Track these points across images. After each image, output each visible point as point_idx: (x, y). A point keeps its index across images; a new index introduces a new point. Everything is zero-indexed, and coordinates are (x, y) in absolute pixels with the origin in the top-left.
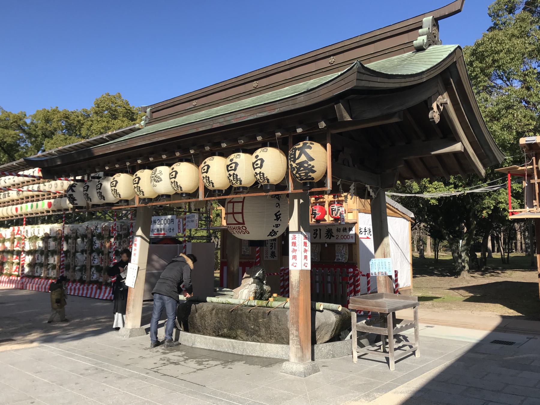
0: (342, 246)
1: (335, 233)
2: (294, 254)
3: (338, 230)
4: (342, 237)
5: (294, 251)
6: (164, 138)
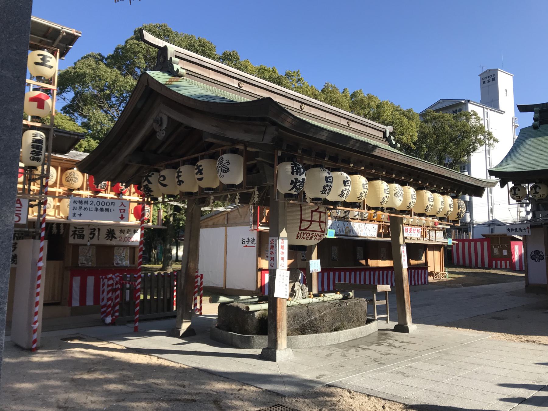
0: (122, 248)
1: (117, 234)
2: (272, 256)
3: (122, 231)
4: (126, 239)
5: (283, 253)
6: (433, 171)
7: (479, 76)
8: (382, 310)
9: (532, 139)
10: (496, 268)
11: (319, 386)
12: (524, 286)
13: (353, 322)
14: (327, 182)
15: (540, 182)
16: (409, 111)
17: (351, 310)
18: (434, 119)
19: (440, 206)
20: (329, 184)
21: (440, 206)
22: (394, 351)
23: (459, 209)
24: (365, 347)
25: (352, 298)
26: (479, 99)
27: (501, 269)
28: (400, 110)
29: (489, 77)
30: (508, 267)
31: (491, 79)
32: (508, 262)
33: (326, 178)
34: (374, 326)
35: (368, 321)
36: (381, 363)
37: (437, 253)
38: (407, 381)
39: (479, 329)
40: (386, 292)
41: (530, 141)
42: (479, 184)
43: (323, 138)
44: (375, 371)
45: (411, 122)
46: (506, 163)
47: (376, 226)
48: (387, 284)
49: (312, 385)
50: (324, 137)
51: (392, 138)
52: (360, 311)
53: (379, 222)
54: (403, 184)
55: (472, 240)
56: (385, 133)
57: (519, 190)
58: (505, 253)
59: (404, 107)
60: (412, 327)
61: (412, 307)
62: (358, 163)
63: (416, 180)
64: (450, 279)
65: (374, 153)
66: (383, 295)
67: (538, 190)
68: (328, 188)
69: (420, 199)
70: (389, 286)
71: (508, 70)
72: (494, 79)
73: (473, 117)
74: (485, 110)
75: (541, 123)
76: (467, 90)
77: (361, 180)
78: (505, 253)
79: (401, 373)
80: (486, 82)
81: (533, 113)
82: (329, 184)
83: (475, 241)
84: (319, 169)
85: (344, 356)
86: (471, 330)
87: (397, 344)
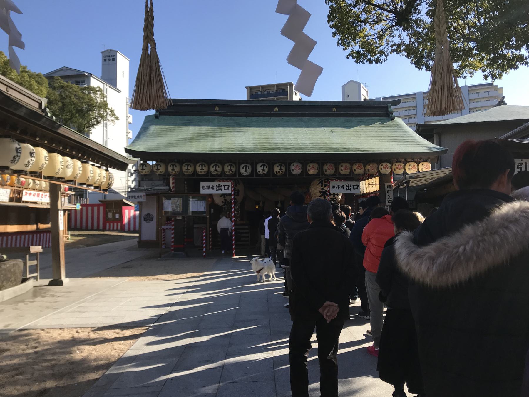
6: (97, 149)
7: (102, 53)
8: (33, 269)
9: (155, 126)
10: (109, 230)
11: (12, 332)
12: (136, 243)
13: (11, 281)
14: (17, 152)
15: (161, 162)
17: (10, 271)
18: (62, 87)
19: (97, 177)
20: (19, 154)
21: (97, 177)
22: (59, 299)
24: (32, 300)
25: (6, 260)
26: (100, 74)
27: (113, 230)
29: (109, 56)
30: (119, 228)
31: (111, 58)
32: (119, 224)
33: (17, 149)
34: (30, 284)
35: (24, 280)
36: (55, 309)
38: (84, 315)
39: (117, 276)
40: (37, 253)
41: (153, 128)
42: (126, 161)
43: (22, 114)
44: (54, 314)
46: (137, 144)
47: (9, 191)
48: (39, 245)
49: (7, 332)
50: (22, 113)
51: (48, 110)
52: (17, 271)
53: (12, 186)
54: (73, 157)
55: (90, 205)
56: (40, 104)
57: (146, 166)
58: (117, 216)
60: (65, 280)
61: (66, 263)
62: (43, 137)
63: (83, 155)
64: (72, 241)
65: (59, 131)
66: (34, 256)
67: (159, 168)
68: (17, 158)
69: (84, 170)
70: (40, 247)
71: (126, 54)
72: (114, 59)
73: (99, 93)
74: (105, 86)
75: (160, 114)
76: (89, 63)
77: (43, 152)
78: (117, 216)
79: (76, 312)
80: (107, 60)
82: (19, 154)
83: (92, 206)
84: (8, 140)
85: (16, 309)
86: (111, 278)
87: (58, 294)
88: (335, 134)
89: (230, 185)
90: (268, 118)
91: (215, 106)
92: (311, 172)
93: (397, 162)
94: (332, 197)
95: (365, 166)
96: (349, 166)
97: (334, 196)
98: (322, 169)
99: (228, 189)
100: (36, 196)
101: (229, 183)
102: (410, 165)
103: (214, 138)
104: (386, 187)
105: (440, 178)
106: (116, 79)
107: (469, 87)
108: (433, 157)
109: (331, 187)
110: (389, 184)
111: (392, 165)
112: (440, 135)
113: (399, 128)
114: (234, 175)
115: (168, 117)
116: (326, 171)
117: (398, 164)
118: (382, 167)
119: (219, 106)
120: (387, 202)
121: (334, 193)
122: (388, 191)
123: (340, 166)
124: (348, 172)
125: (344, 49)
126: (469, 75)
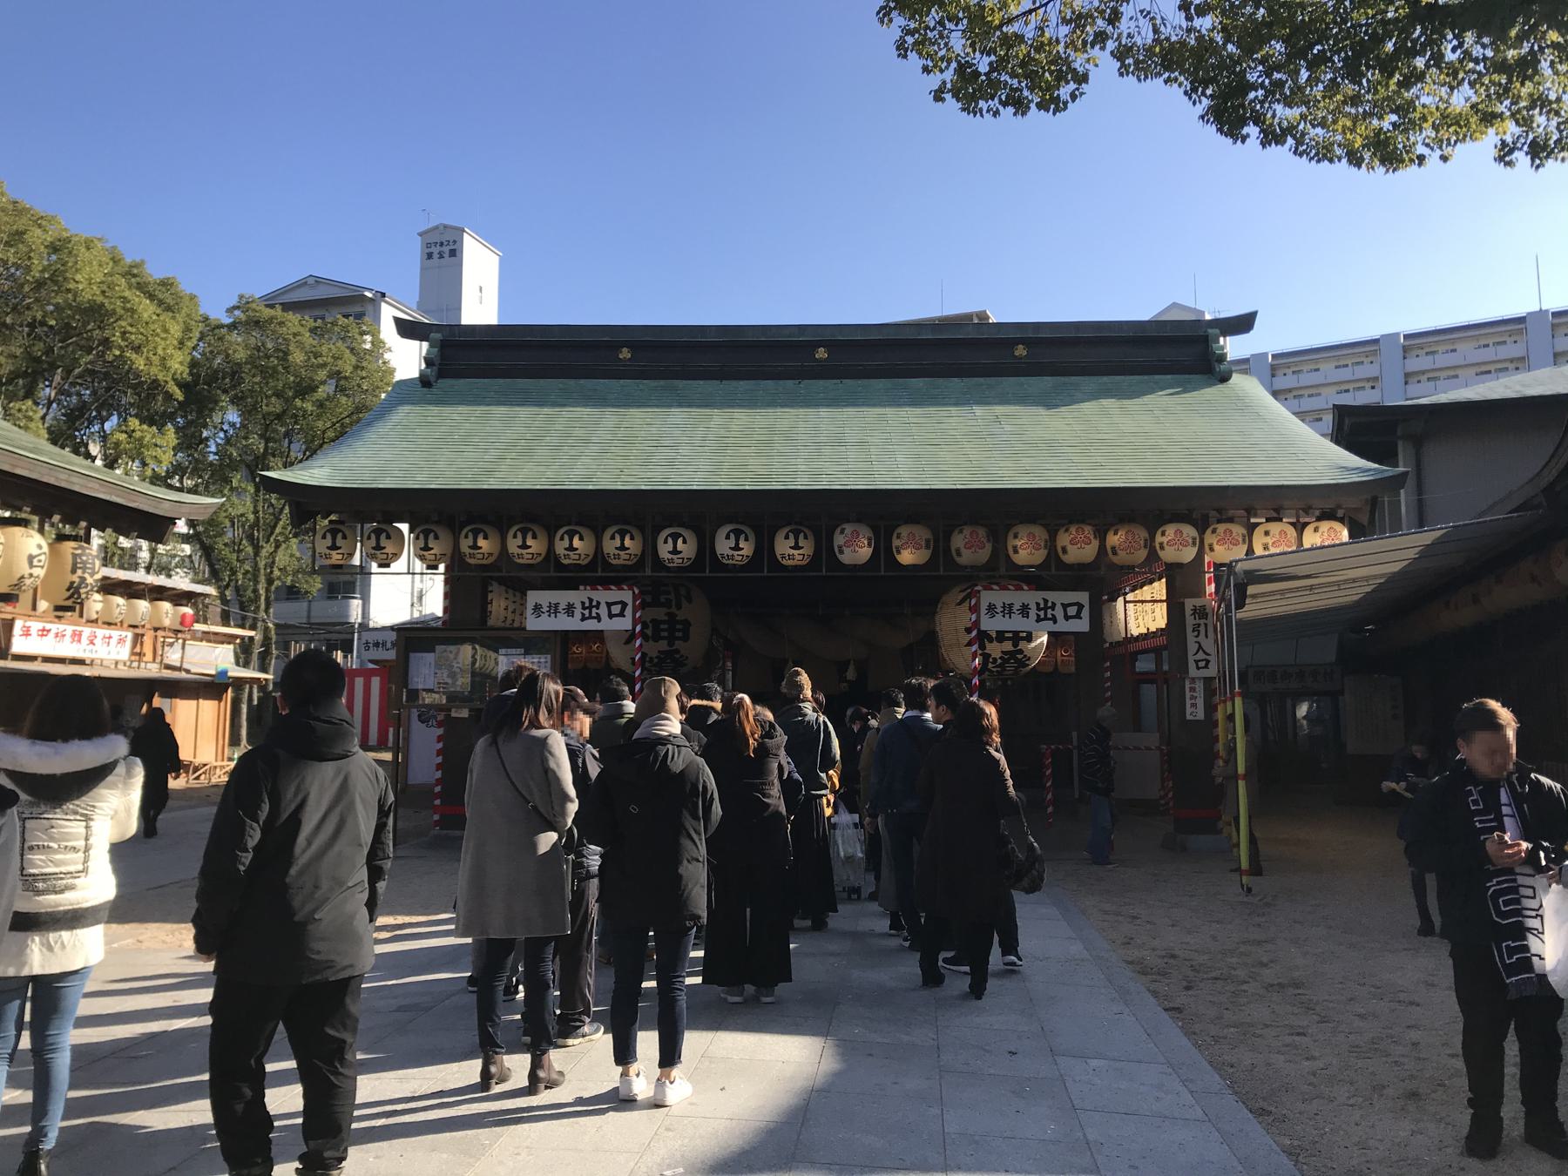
7: (420, 234)
16: (166, 284)
23: (74, 571)
28: (135, 276)
31: (446, 249)
37: (208, 707)
45: (166, 316)
59: (155, 271)
71: (490, 238)
72: (455, 253)
75: (442, 374)
80: (436, 256)
81: (425, 345)
88: (1008, 428)
89: (629, 600)
90: (790, 383)
91: (616, 346)
92: (907, 557)
93: (1219, 521)
94: (1008, 646)
95: (1101, 535)
96: (1040, 533)
97: (1015, 645)
98: (947, 550)
99: (621, 614)
100: (68, 638)
101: (627, 596)
102: (1267, 533)
103: (587, 442)
104: (1188, 611)
105: (1393, 579)
106: (459, 309)
107: (1554, 314)
108: (1352, 502)
109: (983, 610)
110: (1198, 602)
111: (1202, 532)
112: (1418, 442)
113: (1243, 405)
114: (640, 563)
115: (462, 383)
116: (959, 554)
117: (1221, 528)
118: (1165, 540)
119: (632, 345)
120: (1192, 665)
121: (1016, 633)
122: (1196, 628)
123: (1011, 535)
124: (1039, 557)
125: (926, 70)
126: (1439, 153)
